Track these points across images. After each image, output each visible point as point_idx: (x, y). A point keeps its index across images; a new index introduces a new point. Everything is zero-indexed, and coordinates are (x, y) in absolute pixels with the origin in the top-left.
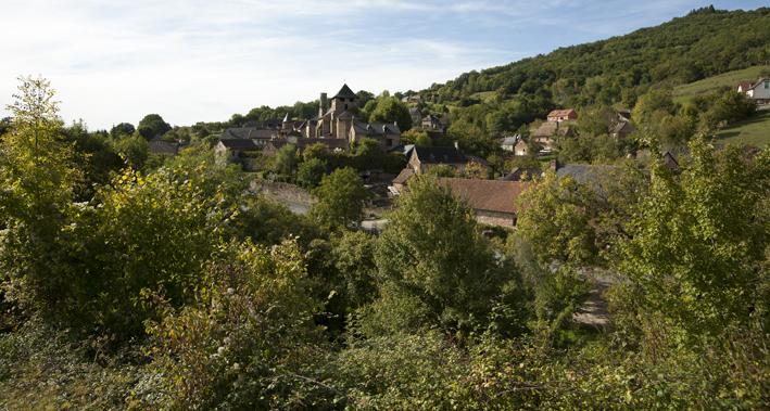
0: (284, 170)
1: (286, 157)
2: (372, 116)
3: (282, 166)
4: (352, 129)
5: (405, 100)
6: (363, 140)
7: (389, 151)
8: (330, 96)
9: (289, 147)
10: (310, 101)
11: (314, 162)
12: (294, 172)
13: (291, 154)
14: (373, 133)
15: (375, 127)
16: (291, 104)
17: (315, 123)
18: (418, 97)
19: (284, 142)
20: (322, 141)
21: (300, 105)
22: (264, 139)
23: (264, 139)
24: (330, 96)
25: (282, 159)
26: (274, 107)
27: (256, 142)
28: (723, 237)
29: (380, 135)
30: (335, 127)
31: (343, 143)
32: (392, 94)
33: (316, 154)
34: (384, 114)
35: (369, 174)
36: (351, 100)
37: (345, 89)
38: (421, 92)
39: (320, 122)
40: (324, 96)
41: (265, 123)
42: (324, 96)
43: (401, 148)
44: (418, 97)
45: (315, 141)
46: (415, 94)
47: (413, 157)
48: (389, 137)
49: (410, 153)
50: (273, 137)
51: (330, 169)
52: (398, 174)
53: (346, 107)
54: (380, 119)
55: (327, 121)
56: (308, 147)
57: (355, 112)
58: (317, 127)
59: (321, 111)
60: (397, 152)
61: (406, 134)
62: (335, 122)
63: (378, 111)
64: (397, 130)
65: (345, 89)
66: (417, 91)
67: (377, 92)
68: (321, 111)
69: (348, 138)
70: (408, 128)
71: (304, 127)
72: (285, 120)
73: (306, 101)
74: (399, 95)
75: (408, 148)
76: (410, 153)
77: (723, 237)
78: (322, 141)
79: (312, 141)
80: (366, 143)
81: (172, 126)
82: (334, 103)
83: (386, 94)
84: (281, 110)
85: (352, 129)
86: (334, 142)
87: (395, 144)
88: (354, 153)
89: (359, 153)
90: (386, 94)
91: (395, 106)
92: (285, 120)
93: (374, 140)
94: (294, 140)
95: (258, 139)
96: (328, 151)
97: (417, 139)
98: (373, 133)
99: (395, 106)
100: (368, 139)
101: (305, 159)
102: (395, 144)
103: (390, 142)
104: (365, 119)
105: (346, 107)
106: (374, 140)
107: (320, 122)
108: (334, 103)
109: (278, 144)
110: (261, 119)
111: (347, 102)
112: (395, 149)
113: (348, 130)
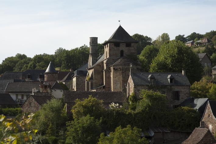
0: (49, 131)
1: (51, 115)
2: (153, 65)
3: (46, 125)
4: (131, 81)
5: (188, 44)
6: (144, 93)
7: (176, 107)
8: (100, 41)
9: (54, 103)
10: (74, 48)
11: (86, 120)
12: (61, 133)
13: (57, 111)
14: (155, 85)
15: (157, 76)
16: (51, 51)
17: (85, 74)
18: (205, 40)
19: (50, 97)
20: (94, 94)
21: (61, 52)
22: (23, 93)
23: (23, 93)
24: (100, 41)
25: (46, 117)
26: (31, 55)
27: (14, 97)
28: (22, 79)
29: (165, 86)
30: (108, 78)
31: (119, 96)
32: (172, 38)
33: (88, 110)
34: (169, 61)
35: (153, 134)
36: (128, 45)
37: (121, 32)
38: (207, 34)
39: (90, 72)
40: (94, 40)
41: (24, 75)
42: (94, 40)
43: (190, 101)
44: (205, 40)
45: (86, 95)
46: (200, 37)
47: (207, 111)
48: (176, 89)
49: (203, 109)
50: (34, 90)
51: (108, 127)
52: (189, 134)
53: (122, 52)
54: (163, 68)
55: (99, 70)
56: (78, 102)
57: (133, 59)
58: (87, 78)
59: (90, 59)
60: (186, 108)
61: (197, 85)
62: (108, 70)
63: (160, 58)
64: (186, 81)
65: (121, 32)
66: (203, 32)
67: (154, 35)
68: (90, 59)
69: (125, 90)
70: (198, 79)
71: (70, 78)
72: (47, 70)
73: (69, 47)
74: (180, 38)
75: (199, 102)
76: (203, 109)
77: (22, 79)
78: (94, 94)
79: (82, 94)
80: (149, 97)
81: (197, 33)
82: (107, 49)
83: (165, 37)
84: (40, 59)
85: (131, 81)
86: (109, 96)
87: (183, 97)
88: (134, 108)
89: (139, 109)
90: (165, 37)
91: (181, 51)
92: (47, 70)
93: (159, 93)
94: (59, 94)
95: (17, 93)
96: (103, 106)
97: (210, 91)
98: (155, 85)
99: (181, 51)
100: (151, 92)
101: (74, 116)
102: (183, 97)
103: (176, 95)
104: (145, 68)
105: (122, 52)
106: (159, 93)
107: (90, 72)
108: (107, 49)
109: (41, 99)
110: (16, 70)
111: (123, 47)
112: (183, 104)
113: (125, 81)
